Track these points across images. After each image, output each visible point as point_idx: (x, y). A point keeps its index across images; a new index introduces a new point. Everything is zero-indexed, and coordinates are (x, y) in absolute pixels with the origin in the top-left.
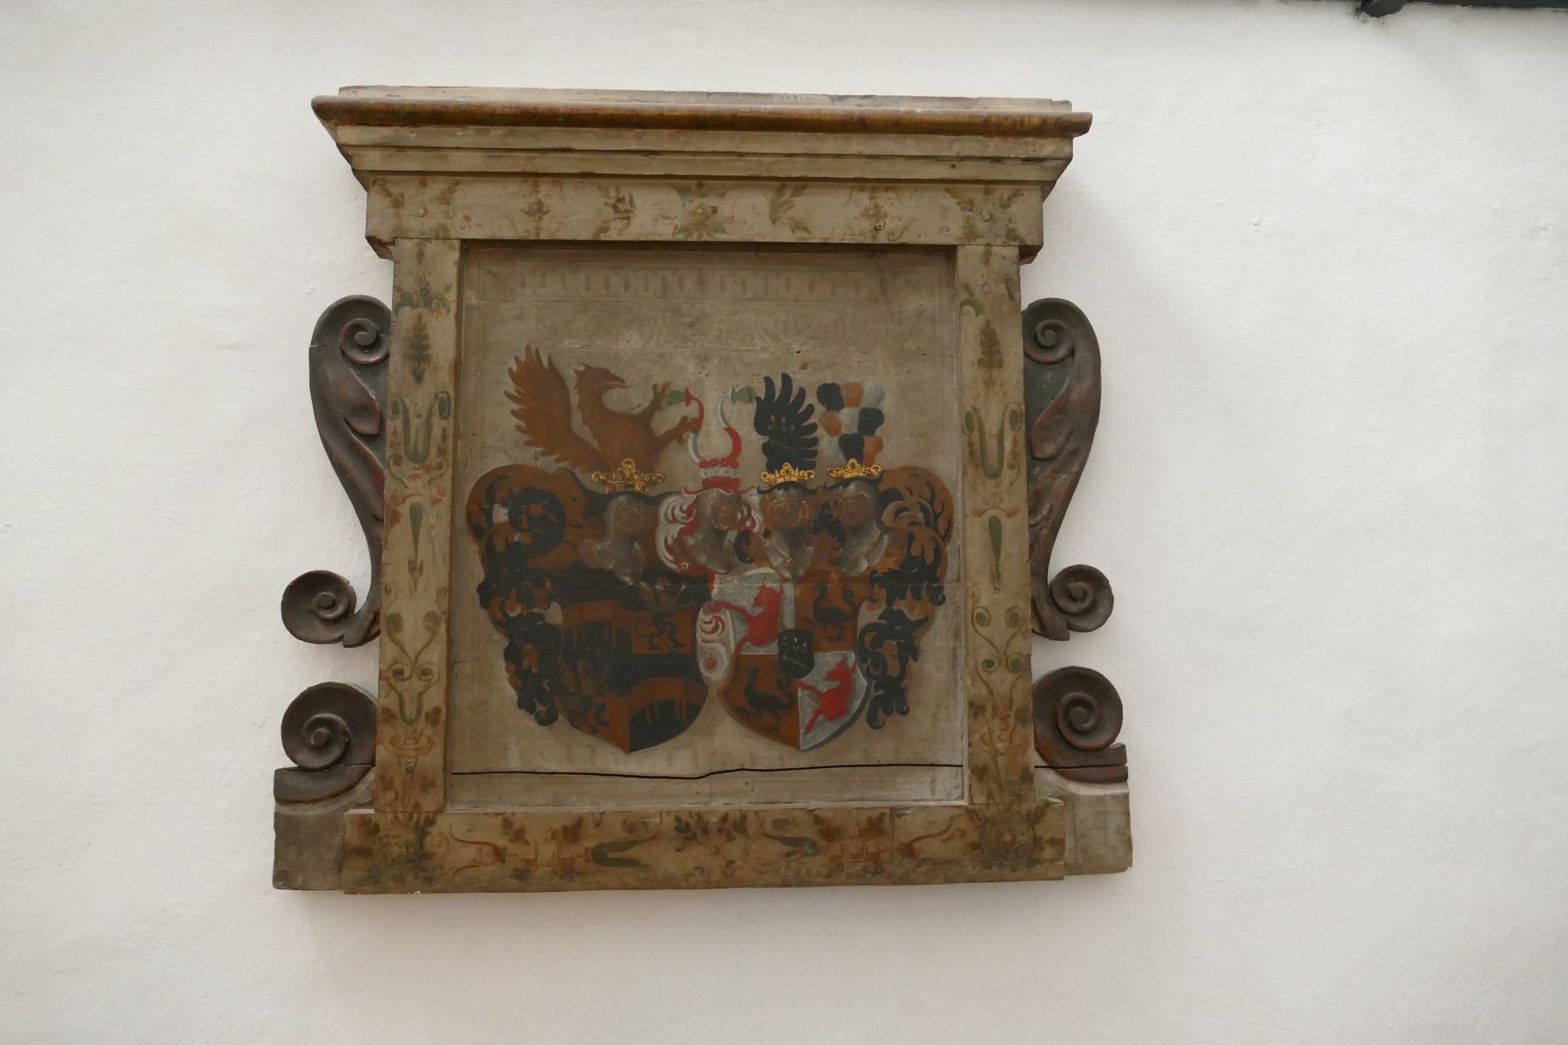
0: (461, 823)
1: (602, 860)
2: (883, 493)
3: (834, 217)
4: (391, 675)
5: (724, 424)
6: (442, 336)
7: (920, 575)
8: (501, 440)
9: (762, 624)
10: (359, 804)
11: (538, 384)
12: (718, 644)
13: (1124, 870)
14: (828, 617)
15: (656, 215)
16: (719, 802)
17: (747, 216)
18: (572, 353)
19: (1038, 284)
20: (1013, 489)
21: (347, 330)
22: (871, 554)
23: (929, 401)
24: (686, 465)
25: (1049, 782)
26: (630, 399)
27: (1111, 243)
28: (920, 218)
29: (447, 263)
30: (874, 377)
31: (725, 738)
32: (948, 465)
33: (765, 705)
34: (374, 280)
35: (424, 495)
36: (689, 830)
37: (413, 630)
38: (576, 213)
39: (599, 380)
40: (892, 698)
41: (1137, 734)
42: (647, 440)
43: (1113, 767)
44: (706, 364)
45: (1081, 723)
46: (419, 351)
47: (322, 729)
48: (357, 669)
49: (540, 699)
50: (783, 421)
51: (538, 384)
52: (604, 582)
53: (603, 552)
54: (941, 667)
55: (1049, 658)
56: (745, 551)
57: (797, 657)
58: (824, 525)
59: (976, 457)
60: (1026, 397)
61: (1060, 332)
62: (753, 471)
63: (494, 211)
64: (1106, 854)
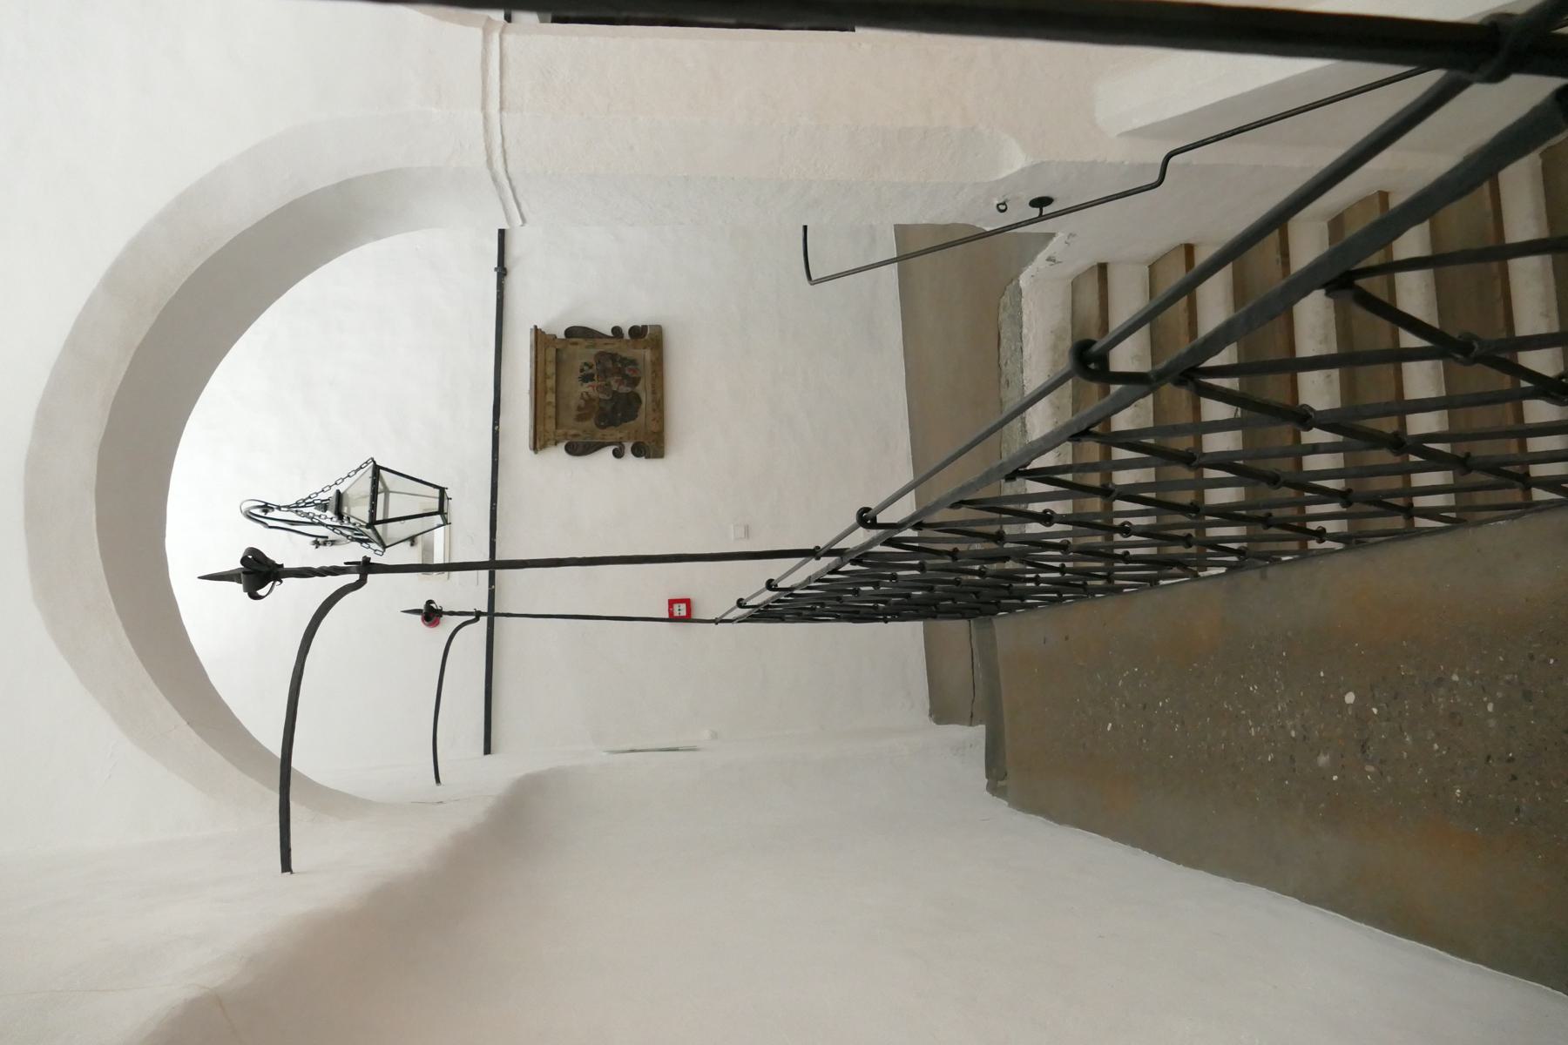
0: (654, 427)
1: (659, 406)
2: (599, 362)
3: (551, 369)
4: (629, 439)
5: (587, 388)
6: (573, 432)
7: (613, 357)
8: (590, 424)
9: (621, 383)
10: (651, 446)
11: (580, 418)
12: (624, 389)
13: (994, 789)
14: (620, 372)
15: (551, 398)
16: (649, 390)
17: (551, 383)
18: (575, 413)
19: (561, 335)
20: (598, 341)
21: (573, 450)
22: (609, 365)
23: (584, 354)
24: (594, 394)
25: (648, 338)
26: (582, 403)
27: (555, 320)
28: (551, 353)
29: (560, 431)
30: (578, 363)
31: (639, 388)
32: (594, 351)
33: (634, 382)
34: (562, 446)
35: (600, 435)
36: (654, 392)
37: (619, 435)
38: (551, 411)
39: (579, 408)
40: (633, 362)
41: (640, 324)
42: (589, 400)
43: (645, 327)
44: (577, 391)
45: (638, 332)
46: (575, 435)
47: (639, 451)
48: (628, 446)
49: (634, 417)
50: (586, 378)
51: (580, 418)
52: (614, 408)
53: (608, 408)
54: (628, 353)
55: (627, 336)
56: (608, 385)
57: (625, 376)
58: (604, 373)
59: (594, 346)
60: (1127, 406)
61: (570, 332)
62: (596, 383)
63: (551, 425)
64: (659, 330)
